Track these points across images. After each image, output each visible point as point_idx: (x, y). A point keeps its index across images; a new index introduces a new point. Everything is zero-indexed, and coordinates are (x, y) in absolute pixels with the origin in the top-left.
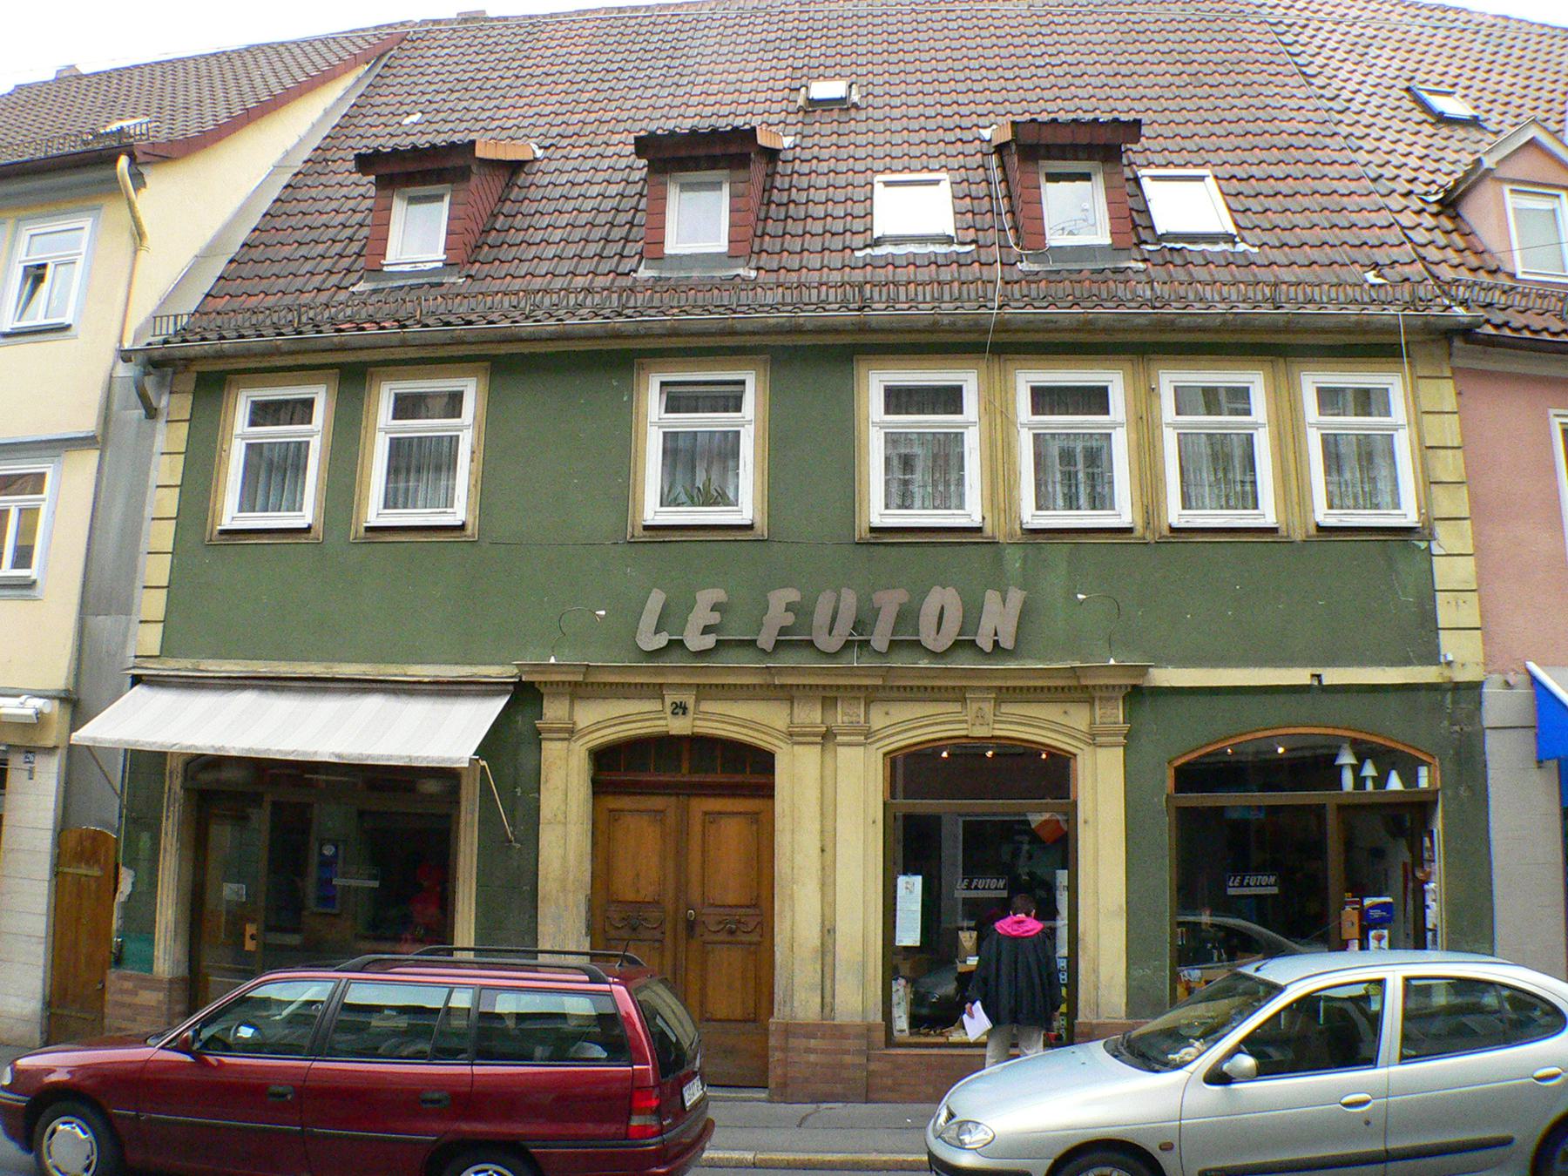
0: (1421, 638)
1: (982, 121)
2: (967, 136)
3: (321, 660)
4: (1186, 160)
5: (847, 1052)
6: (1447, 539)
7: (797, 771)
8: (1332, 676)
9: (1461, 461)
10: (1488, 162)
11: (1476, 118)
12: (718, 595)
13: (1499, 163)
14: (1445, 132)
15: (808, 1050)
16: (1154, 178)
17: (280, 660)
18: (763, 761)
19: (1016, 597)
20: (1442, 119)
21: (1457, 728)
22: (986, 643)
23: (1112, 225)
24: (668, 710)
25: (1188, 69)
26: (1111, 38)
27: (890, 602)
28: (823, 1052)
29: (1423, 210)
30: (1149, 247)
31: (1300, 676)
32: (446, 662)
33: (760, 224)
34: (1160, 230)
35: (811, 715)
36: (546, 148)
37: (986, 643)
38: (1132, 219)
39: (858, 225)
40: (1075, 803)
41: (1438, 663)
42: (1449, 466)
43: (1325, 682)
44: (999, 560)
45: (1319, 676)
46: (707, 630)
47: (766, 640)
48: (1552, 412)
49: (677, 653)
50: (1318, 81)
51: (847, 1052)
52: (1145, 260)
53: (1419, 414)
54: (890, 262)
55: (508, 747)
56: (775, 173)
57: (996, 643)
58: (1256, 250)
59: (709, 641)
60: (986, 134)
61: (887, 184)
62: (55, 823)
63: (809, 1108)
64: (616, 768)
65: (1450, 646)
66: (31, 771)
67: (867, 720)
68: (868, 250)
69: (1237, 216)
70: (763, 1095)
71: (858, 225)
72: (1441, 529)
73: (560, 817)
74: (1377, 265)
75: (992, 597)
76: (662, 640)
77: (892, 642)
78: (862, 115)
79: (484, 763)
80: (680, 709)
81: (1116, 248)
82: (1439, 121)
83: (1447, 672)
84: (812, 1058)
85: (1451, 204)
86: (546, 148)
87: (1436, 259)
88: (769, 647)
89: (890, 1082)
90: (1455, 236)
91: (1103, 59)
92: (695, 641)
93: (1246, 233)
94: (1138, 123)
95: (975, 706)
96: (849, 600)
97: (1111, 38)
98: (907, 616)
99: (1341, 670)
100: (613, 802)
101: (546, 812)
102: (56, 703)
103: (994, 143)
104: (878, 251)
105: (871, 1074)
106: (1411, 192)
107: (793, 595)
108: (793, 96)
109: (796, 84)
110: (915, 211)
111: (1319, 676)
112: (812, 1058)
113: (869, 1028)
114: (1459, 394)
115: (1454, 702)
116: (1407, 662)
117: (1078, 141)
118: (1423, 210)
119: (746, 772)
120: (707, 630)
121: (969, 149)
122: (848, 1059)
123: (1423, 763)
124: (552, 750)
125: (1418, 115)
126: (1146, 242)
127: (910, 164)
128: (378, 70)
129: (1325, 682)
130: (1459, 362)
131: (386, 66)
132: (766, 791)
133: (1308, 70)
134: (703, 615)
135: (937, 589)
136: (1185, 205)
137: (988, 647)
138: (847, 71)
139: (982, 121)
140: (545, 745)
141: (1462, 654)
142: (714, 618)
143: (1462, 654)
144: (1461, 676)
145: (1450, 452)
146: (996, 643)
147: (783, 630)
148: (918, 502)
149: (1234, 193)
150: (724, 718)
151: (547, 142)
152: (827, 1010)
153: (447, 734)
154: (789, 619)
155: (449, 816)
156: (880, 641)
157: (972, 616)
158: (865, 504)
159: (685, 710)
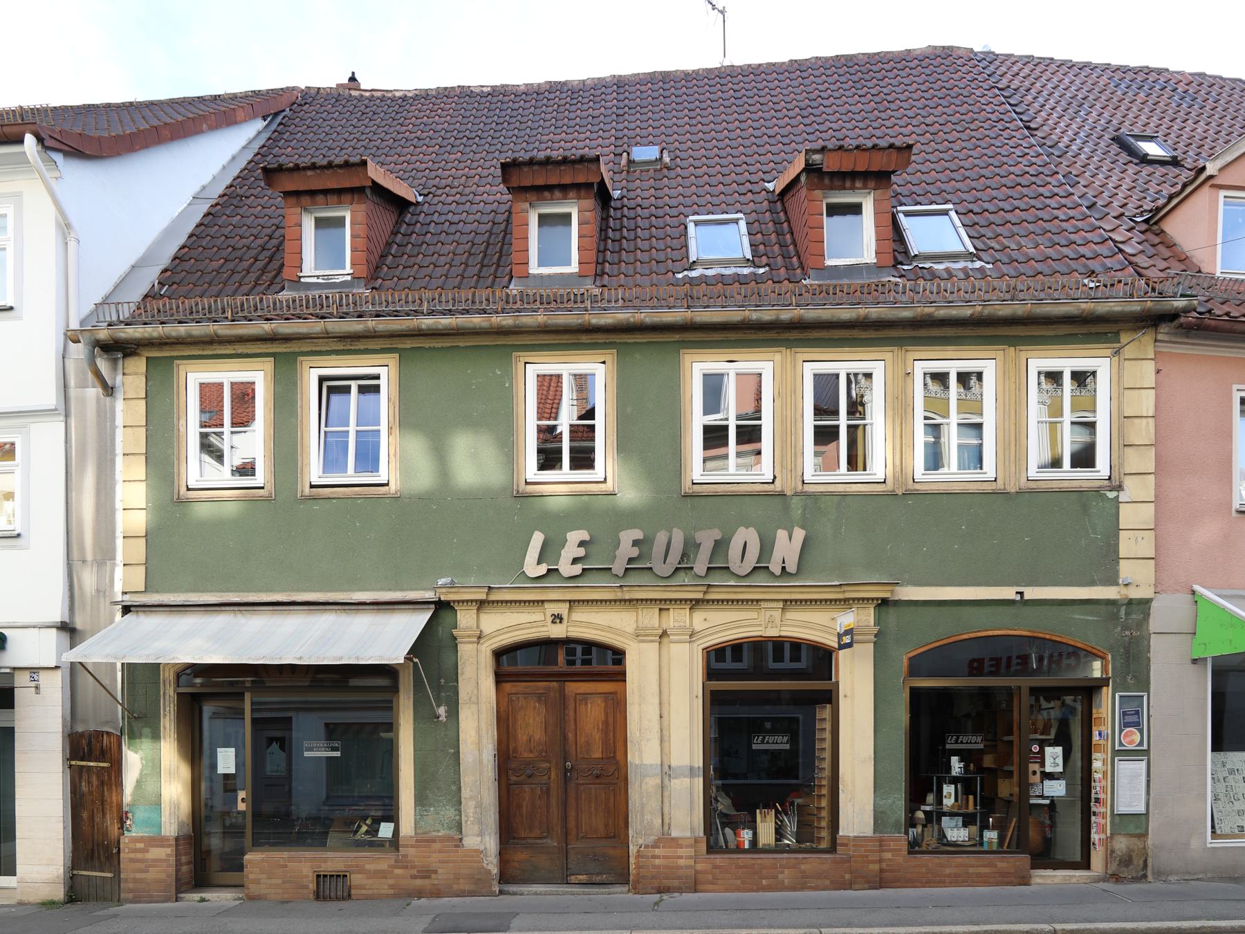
0: (1105, 564)
1: (767, 177)
2: (756, 188)
3: (283, 591)
4: (930, 197)
5: (681, 857)
6: (1134, 489)
7: (641, 666)
8: (1032, 593)
9: (1152, 430)
10: (1211, 168)
11: (1174, 158)
12: (584, 535)
13: (1220, 170)
14: (1149, 169)
15: (654, 857)
16: (907, 214)
17: (249, 591)
18: (618, 655)
19: (799, 534)
20: (1145, 160)
21: (1127, 633)
22: (776, 568)
23: (878, 245)
24: (550, 619)
25: (931, 129)
26: (866, 107)
27: (707, 539)
28: (665, 857)
29: (1133, 228)
30: (906, 267)
31: (1008, 593)
32: (382, 589)
33: (599, 267)
34: (914, 251)
35: (650, 618)
36: (425, 195)
37: (776, 568)
38: (894, 236)
39: (677, 255)
40: (837, 683)
41: (1117, 584)
42: (1143, 432)
43: (1026, 597)
44: (786, 508)
45: (1021, 593)
46: (575, 561)
47: (618, 567)
48: (1235, 387)
49: (554, 576)
50: (1039, 134)
51: (681, 857)
52: (901, 276)
53: (1120, 389)
54: (703, 280)
55: (434, 649)
56: (609, 216)
57: (784, 568)
58: (990, 266)
59: (577, 569)
60: (770, 186)
61: (697, 223)
62: (64, 726)
63: (656, 897)
64: (511, 662)
65: (1126, 570)
66: (37, 688)
67: (691, 624)
68: (686, 273)
69: (975, 241)
70: (625, 888)
71: (677, 255)
72: (1128, 482)
73: (474, 699)
74: (1093, 272)
75: (782, 534)
76: (542, 570)
77: (709, 568)
78: (672, 174)
79: (416, 660)
80: (557, 618)
81: (879, 267)
82: (1142, 162)
83: (1124, 591)
84: (657, 862)
85: (1153, 222)
86: (425, 195)
87: (1146, 265)
88: (621, 573)
89: (710, 877)
90: (1160, 247)
91: (862, 125)
92: (566, 569)
93: (982, 254)
94: (910, 147)
95: (768, 613)
96: (678, 538)
97: (866, 107)
98: (720, 546)
99: (1056, 589)
100: (508, 687)
101: (463, 696)
102: (54, 630)
103: (777, 192)
104: (694, 274)
105: (697, 872)
106: (1122, 214)
107: (638, 534)
108: (617, 160)
109: (619, 150)
110: (720, 243)
111: (1021, 593)
112: (657, 862)
113: (696, 840)
114: (1158, 372)
115: (1127, 614)
116: (1092, 583)
117: (858, 169)
118: (1133, 228)
119: (603, 662)
120: (575, 561)
121: (759, 198)
122: (682, 862)
123: (1096, 656)
124: (466, 650)
125: (1124, 157)
126: (902, 264)
127: (715, 203)
128: (274, 126)
129: (1026, 597)
130: (1165, 348)
131: (280, 124)
132: (620, 677)
133: (1033, 125)
134: (571, 550)
135: (742, 528)
136: (936, 234)
137: (778, 571)
138: (657, 140)
139: (767, 177)
140: (460, 647)
141: (1136, 577)
142: (581, 552)
143: (1136, 577)
144: (1135, 594)
145: (1144, 420)
146: (784, 568)
147: (630, 560)
148: (168, 676)
149: (972, 221)
150: (589, 625)
151: (425, 192)
152: (666, 828)
153: (386, 639)
154: (635, 552)
155: (391, 702)
156: (700, 567)
157: (766, 547)
158: (688, 470)
159: (561, 620)
